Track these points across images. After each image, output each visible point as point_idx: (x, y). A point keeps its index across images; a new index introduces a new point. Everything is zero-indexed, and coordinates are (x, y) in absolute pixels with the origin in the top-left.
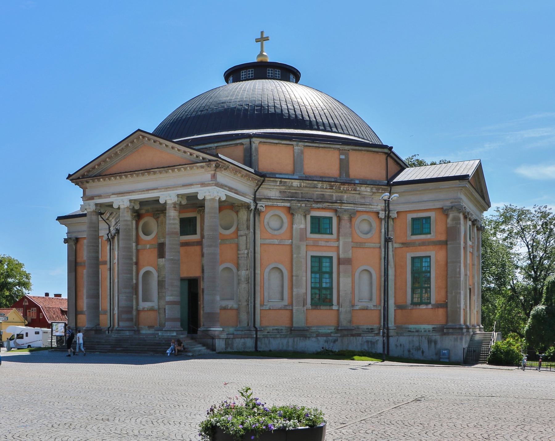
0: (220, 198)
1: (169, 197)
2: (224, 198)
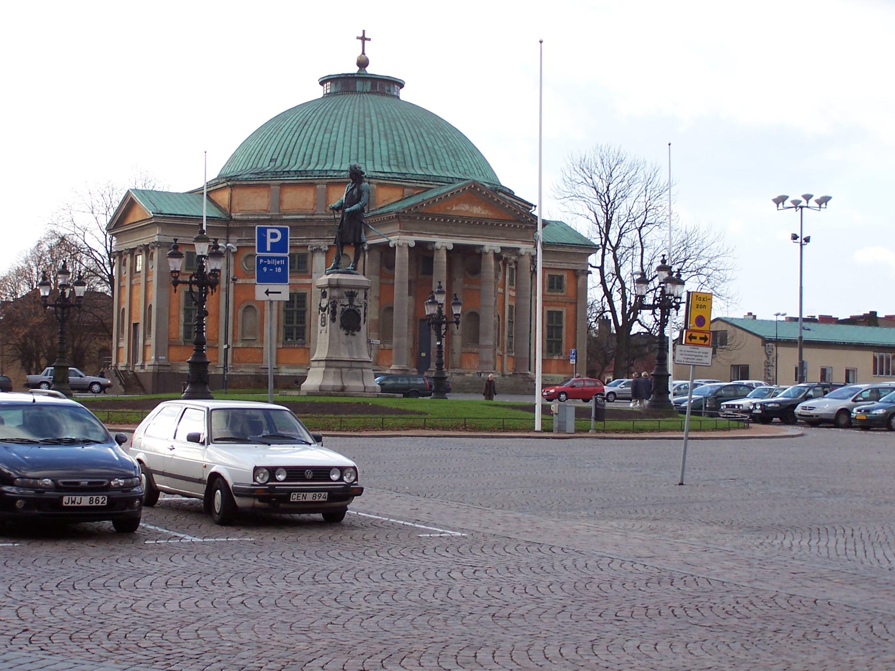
0: (495, 253)
1: (491, 246)
2: (451, 247)
